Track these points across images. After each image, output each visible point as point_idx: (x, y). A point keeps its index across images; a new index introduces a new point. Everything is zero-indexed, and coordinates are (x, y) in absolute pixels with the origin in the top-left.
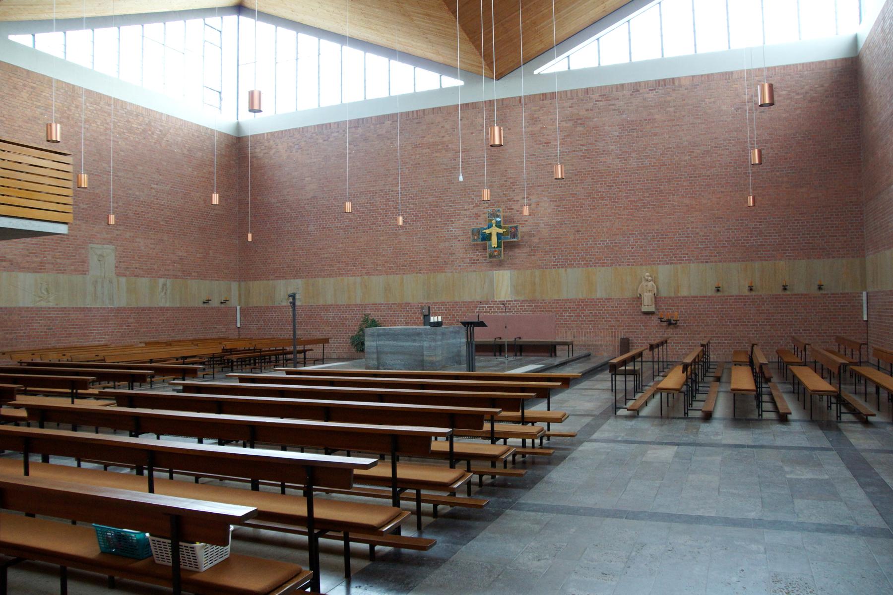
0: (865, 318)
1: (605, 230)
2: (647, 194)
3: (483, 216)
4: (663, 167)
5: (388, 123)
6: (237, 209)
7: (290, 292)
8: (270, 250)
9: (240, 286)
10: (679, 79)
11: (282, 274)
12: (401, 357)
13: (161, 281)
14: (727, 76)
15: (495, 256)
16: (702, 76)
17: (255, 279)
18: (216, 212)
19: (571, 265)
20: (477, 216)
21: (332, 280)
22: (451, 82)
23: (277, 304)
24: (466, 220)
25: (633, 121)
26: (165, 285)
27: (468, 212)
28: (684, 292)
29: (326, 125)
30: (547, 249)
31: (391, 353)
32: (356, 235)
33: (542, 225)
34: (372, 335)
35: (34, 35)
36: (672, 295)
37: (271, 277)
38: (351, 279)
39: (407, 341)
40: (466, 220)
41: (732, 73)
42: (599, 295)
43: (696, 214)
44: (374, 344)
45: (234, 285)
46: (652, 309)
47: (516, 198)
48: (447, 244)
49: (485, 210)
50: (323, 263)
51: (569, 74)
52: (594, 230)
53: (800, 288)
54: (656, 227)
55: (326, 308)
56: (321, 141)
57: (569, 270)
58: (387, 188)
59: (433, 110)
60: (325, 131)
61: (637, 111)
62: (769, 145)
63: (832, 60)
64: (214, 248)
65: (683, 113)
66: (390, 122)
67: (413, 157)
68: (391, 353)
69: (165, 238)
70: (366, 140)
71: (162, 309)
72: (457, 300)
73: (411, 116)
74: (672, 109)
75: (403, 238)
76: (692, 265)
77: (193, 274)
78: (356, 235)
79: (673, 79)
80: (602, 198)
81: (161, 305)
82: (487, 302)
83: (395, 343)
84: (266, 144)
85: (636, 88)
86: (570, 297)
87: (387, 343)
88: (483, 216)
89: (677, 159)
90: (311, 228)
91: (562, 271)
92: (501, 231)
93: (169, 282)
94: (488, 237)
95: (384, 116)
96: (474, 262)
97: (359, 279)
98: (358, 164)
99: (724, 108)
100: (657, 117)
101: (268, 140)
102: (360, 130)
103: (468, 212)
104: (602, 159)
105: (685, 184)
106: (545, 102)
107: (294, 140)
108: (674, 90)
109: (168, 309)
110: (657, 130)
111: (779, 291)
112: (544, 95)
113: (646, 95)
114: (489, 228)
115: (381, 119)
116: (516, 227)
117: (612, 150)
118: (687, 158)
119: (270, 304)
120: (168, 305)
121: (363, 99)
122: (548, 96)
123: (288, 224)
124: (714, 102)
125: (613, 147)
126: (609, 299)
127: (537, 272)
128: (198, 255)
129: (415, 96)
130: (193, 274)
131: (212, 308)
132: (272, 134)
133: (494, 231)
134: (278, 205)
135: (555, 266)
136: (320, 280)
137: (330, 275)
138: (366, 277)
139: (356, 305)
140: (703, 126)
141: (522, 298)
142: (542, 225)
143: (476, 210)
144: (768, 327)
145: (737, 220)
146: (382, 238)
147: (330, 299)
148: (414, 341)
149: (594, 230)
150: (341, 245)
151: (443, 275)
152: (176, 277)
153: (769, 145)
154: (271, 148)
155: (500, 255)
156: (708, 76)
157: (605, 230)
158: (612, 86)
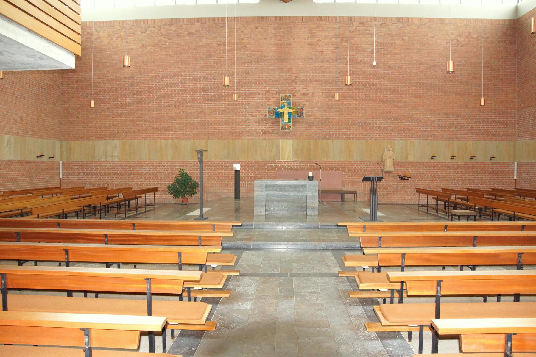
0: (515, 178)
1: (361, 115)
2: (389, 93)
3: (272, 99)
4: (400, 76)
6: (60, 81)
7: (199, 148)
8: (91, 116)
9: (61, 145)
10: (412, 19)
11: (100, 135)
12: (285, 204)
13: (7, 137)
14: (442, 21)
15: (286, 129)
16: (426, 19)
17: (77, 139)
18: (46, 82)
19: (336, 138)
20: (268, 99)
21: (147, 142)
23: (96, 160)
24: (259, 101)
26: (9, 141)
27: (261, 96)
28: (411, 159)
29: (144, 20)
30: (320, 125)
31: (276, 201)
32: (169, 108)
33: (316, 109)
34: (261, 186)
36: (404, 161)
37: (91, 138)
38: (164, 141)
39: (293, 191)
40: (259, 101)
41: (445, 19)
42: (355, 160)
43: (420, 108)
44: (263, 194)
45: (58, 143)
46: (392, 169)
47: (298, 88)
48: (244, 118)
49: (274, 95)
50: (139, 128)
52: (353, 115)
53: (479, 159)
54: (395, 115)
55: (141, 164)
57: (335, 141)
58: (196, 73)
59: (240, 19)
60: (143, 25)
61: (384, 36)
62: (465, 68)
63: (503, 20)
64: (45, 112)
65: (414, 42)
66: (199, 24)
67: (218, 52)
68: (276, 201)
69: (10, 100)
71: (7, 161)
72: (251, 159)
74: (407, 38)
75: (208, 112)
76: (416, 141)
77: (30, 133)
78: (169, 108)
79: (408, 18)
80: (359, 93)
81: (7, 158)
82: (274, 162)
83: (281, 193)
84: (88, 30)
85: (384, 21)
86: (335, 160)
87: (274, 193)
88: (272, 99)
89: (409, 71)
90: (129, 100)
91: (330, 141)
92: (291, 111)
93: (12, 138)
94: (282, 115)
95: (195, 19)
96: (264, 133)
97: (170, 142)
99: (439, 41)
100: (397, 42)
101: (91, 28)
102: (174, 28)
103: (261, 96)
104: (360, 66)
105: (413, 88)
106: (321, 22)
107: (115, 30)
108: (408, 26)
109: (11, 162)
110: (397, 51)
111: (468, 160)
112: (321, 17)
113: (390, 27)
114: (281, 108)
115: (192, 21)
116: (302, 109)
117: (367, 61)
118: (416, 71)
119: (90, 160)
120: (12, 158)
122: (323, 19)
123: (108, 96)
125: (368, 59)
126: (362, 162)
127: (312, 142)
128: (34, 117)
130: (30, 133)
131: (43, 162)
132: (95, 23)
133: (286, 110)
134: (99, 80)
135: (325, 138)
136: (136, 141)
137: (145, 138)
138: (176, 141)
139: (167, 162)
140: (426, 51)
141: (300, 160)
142: (316, 109)
143: (267, 94)
144: (461, 183)
145: (445, 114)
146: (190, 111)
147: (144, 157)
148: (299, 191)
149: (353, 115)
150: (155, 115)
151: (240, 141)
152: (18, 134)
153: (465, 68)
154: (91, 34)
155: (289, 128)
156: (431, 19)
157: (361, 115)
158: (368, 18)
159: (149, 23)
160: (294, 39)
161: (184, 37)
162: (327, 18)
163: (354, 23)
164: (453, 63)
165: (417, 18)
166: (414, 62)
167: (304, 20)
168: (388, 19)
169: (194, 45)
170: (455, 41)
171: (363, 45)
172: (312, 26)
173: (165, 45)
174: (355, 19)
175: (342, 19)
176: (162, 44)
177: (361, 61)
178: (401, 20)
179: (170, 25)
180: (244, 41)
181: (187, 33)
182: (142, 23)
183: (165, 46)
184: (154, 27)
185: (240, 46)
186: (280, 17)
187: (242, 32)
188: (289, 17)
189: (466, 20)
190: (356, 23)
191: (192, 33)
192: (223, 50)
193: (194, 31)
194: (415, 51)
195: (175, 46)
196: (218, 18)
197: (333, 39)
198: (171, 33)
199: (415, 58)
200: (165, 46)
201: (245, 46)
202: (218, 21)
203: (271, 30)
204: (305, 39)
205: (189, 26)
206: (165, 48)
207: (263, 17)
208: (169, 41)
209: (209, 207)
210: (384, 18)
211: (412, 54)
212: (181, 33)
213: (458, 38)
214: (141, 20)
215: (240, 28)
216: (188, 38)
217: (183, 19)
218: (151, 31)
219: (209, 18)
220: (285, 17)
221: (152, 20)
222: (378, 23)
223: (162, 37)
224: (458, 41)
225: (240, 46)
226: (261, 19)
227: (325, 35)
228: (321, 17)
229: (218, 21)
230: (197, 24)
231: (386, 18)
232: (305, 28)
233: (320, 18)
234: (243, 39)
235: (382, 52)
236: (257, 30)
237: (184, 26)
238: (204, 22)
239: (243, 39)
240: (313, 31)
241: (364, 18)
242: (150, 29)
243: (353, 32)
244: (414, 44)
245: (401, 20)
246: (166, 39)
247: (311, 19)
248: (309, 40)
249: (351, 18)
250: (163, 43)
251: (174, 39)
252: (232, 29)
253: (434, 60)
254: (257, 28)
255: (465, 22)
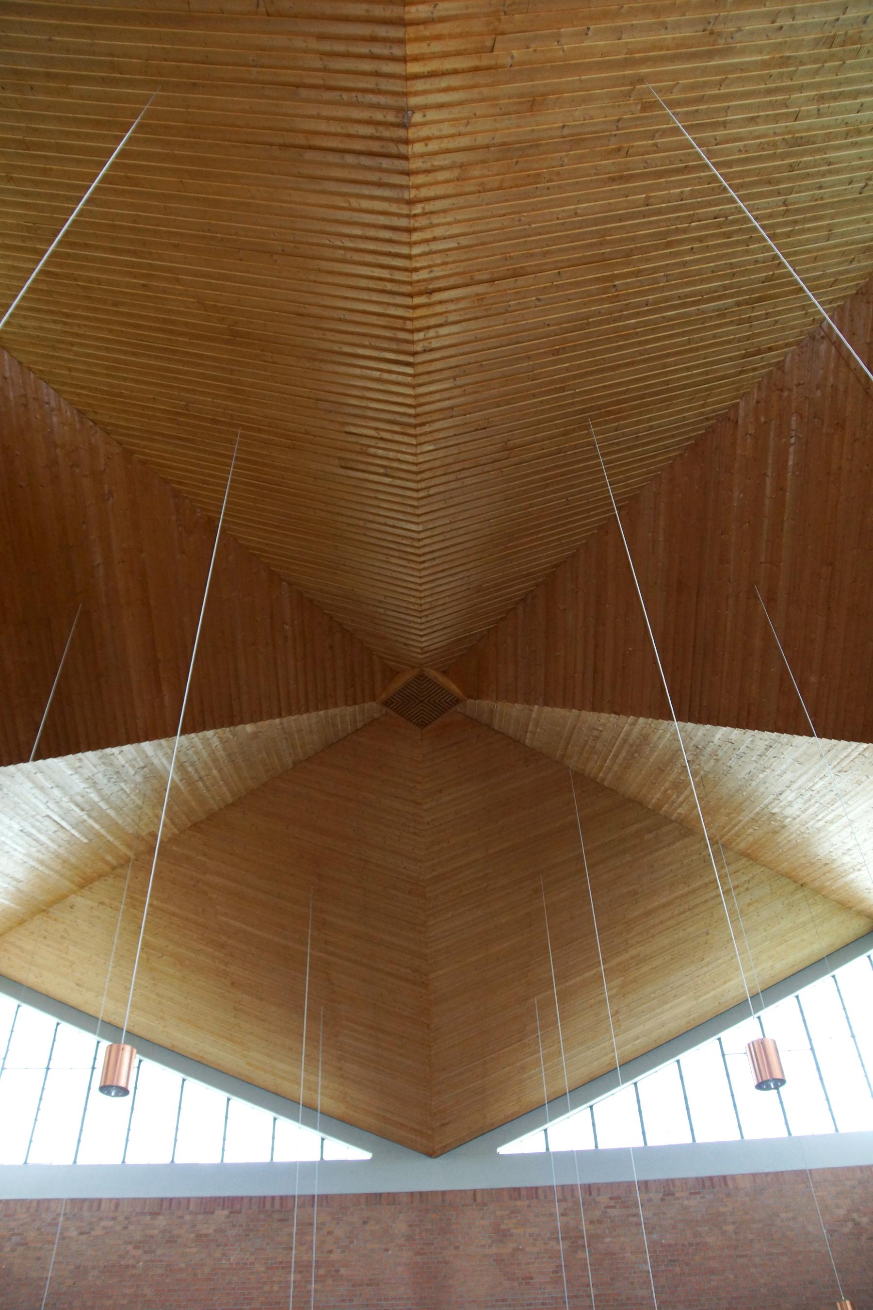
5: (221, 1214)
10: (733, 1177)
14: (802, 1175)
16: (767, 1174)
22: (342, 1151)
25: (670, 1246)
29: (91, 1201)
35: (173, 1161)
51: (546, 1158)
56: (73, 1233)
59: (325, 1199)
60: (86, 1214)
61: (675, 1227)
65: (750, 1236)
66: (226, 1212)
67: (266, 1288)
70: (172, 1241)
73: (268, 1206)
74: (730, 1228)
85: (668, 1189)
95: (215, 1199)
98: (148, 1291)
100: (710, 1240)
102: (161, 1221)
106: (518, 1203)
107: (13, 1224)
108: (728, 1195)
112: (517, 1190)
113: (686, 1202)
115: (208, 1205)
121: (168, 1161)
122: (524, 1193)
124: (794, 1219)
129: (271, 1169)
140: (785, 1259)
156: (777, 1175)
159: (103, 1207)
160: (457, 1248)
161: (186, 1246)
162: (534, 1192)
163: (598, 1199)
164: (852, 1304)
165: (743, 1175)
166: (762, 1290)
167: (479, 1199)
168: (677, 1184)
169: (207, 1270)
170: (850, 1225)
171: (628, 1255)
172: (497, 1213)
173: (134, 1267)
174: (599, 1190)
175: (568, 1191)
176: (127, 1266)
177: (628, 1299)
178: (708, 1183)
179: (154, 1214)
180: (333, 1257)
181: (192, 1236)
182: (86, 1204)
183: (134, 1271)
184: (114, 1219)
185: (322, 1272)
186: (421, 1193)
187: (329, 1233)
188: (444, 1193)
189: (861, 1168)
190: (604, 1199)
191: (206, 1235)
192: (280, 1282)
193: (211, 1231)
194: (757, 1260)
195: (159, 1271)
196: (273, 1198)
197: (552, 1243)
198: (152, 1237)
199: (762, 1281)
200: (134, 1271)
201: (337, 1271)
202: (273, 1205)
203: (401, 1227)
204: (483, 1246)
205: (200, 1217)
206: (133, 1276)
207: (380, 1194)
208: (146, 1257)
209: (521, 1198)
210: (667, 1180)
211: (753, 1270)
212: (179, 1236)
213: (855, 1216)
214: (84, 1200)
215: (323, 1224)
216: (194, 1250)
217: (188, 1200)
218: (104, 1228)
219: (251, 1198)
220: (432, 1192)
221: (111, 1200)
222: (656, 1196)
223: (130, 1247)
224: (857, 1224)
225: (322, 1272)
226: (375, 1199)
227: (531, 1235)
228: (519, 1189)
229: (273, 1205)
230: (221, 1214)
231: (673, 1180)
232: (483, 1218)
233: (516, 1193)
234: (330, 1252)
235: (678, 1270)
236: (367, 1227)
237: (188, 1218)
238: (237, 1207)
239: (330, 1252)
240: (503, 1227)
241: (619, 1184)
242: (103, 1224)
243: (600, 1222)
244: (751, 1241)
245: (708, 1183)
246: (139, 1252)
247: (496, 1195)
248: (494, 1250)
249: (588, 1189)
250: (131, 1262)
251: (159, 1252)
252: (305, 1225)
253: (811, 1282)
254: (365, 1223)
255: (858, 1175)
